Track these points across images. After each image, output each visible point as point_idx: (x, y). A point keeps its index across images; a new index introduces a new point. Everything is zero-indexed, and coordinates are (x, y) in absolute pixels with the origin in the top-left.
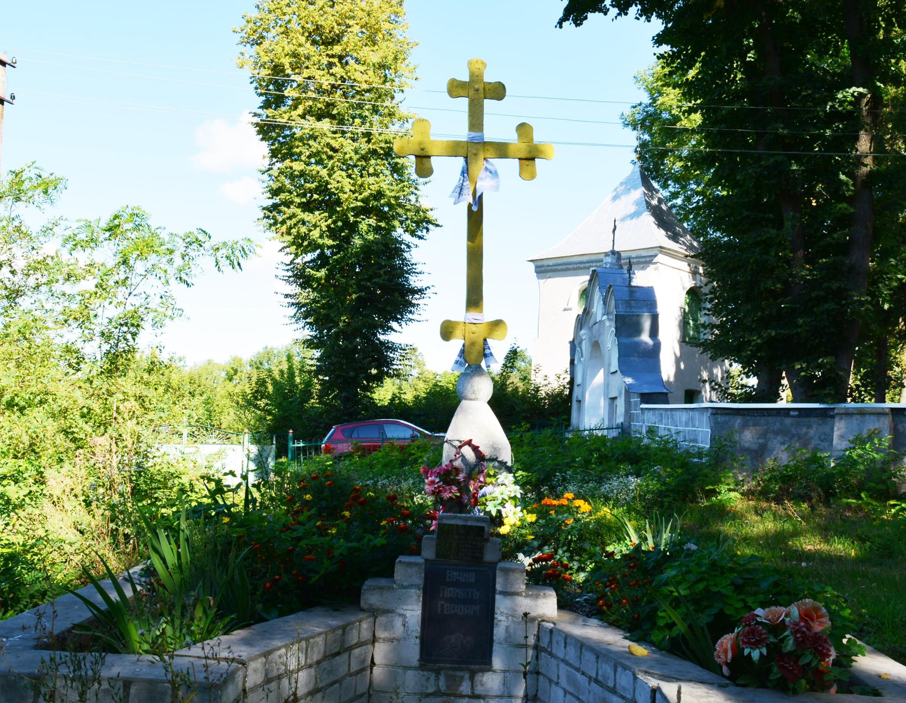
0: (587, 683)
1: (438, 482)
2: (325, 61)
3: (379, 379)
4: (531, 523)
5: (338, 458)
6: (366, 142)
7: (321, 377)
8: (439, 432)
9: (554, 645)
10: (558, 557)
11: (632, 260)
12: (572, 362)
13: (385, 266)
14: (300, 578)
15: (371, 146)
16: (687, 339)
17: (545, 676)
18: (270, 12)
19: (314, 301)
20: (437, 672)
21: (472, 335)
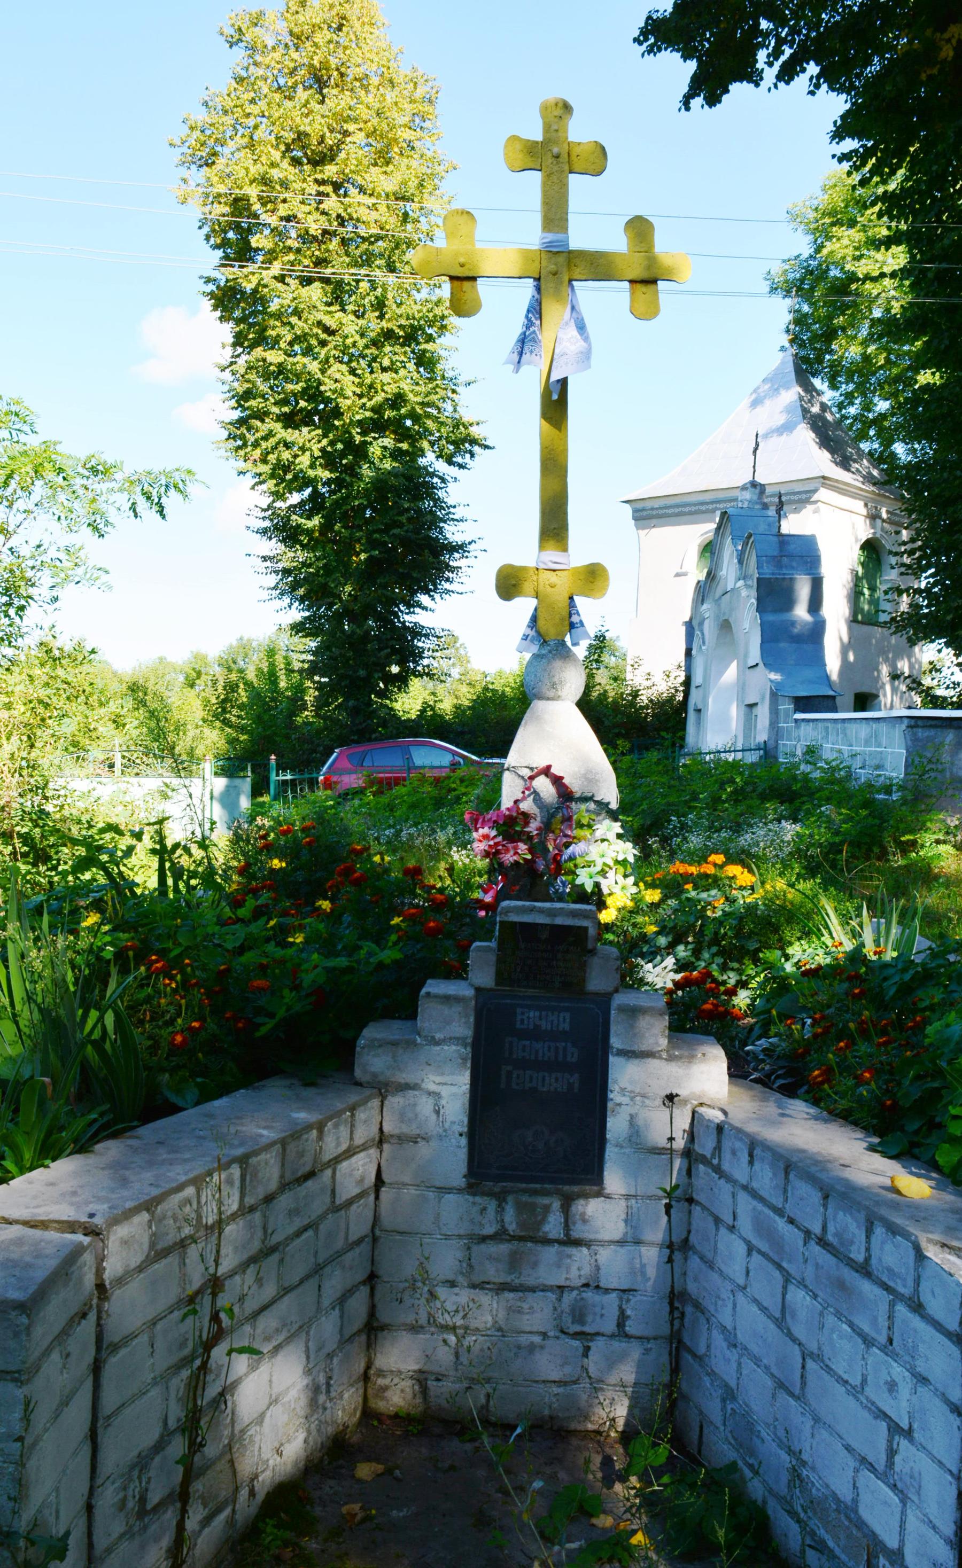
0: (801, 1243)
1: (495, 837)
2: (313, 189)
3: (402, 681)
4: (652, 904)
5: (345, 796)
6: (377, 318)
7: (317, 678)
8: (492, 757)
9: (726, 1155)
10: (703, 964)
11: (784, 499)
12: (688, 653)
13: (408, 510)
14: (240, 1025)
15: (384, 324)
16: (860, 617)
17: (704, 1208)
18: (226, 112)
19: (304, 564)
20: (501, 1198)
21: (549, 589)
